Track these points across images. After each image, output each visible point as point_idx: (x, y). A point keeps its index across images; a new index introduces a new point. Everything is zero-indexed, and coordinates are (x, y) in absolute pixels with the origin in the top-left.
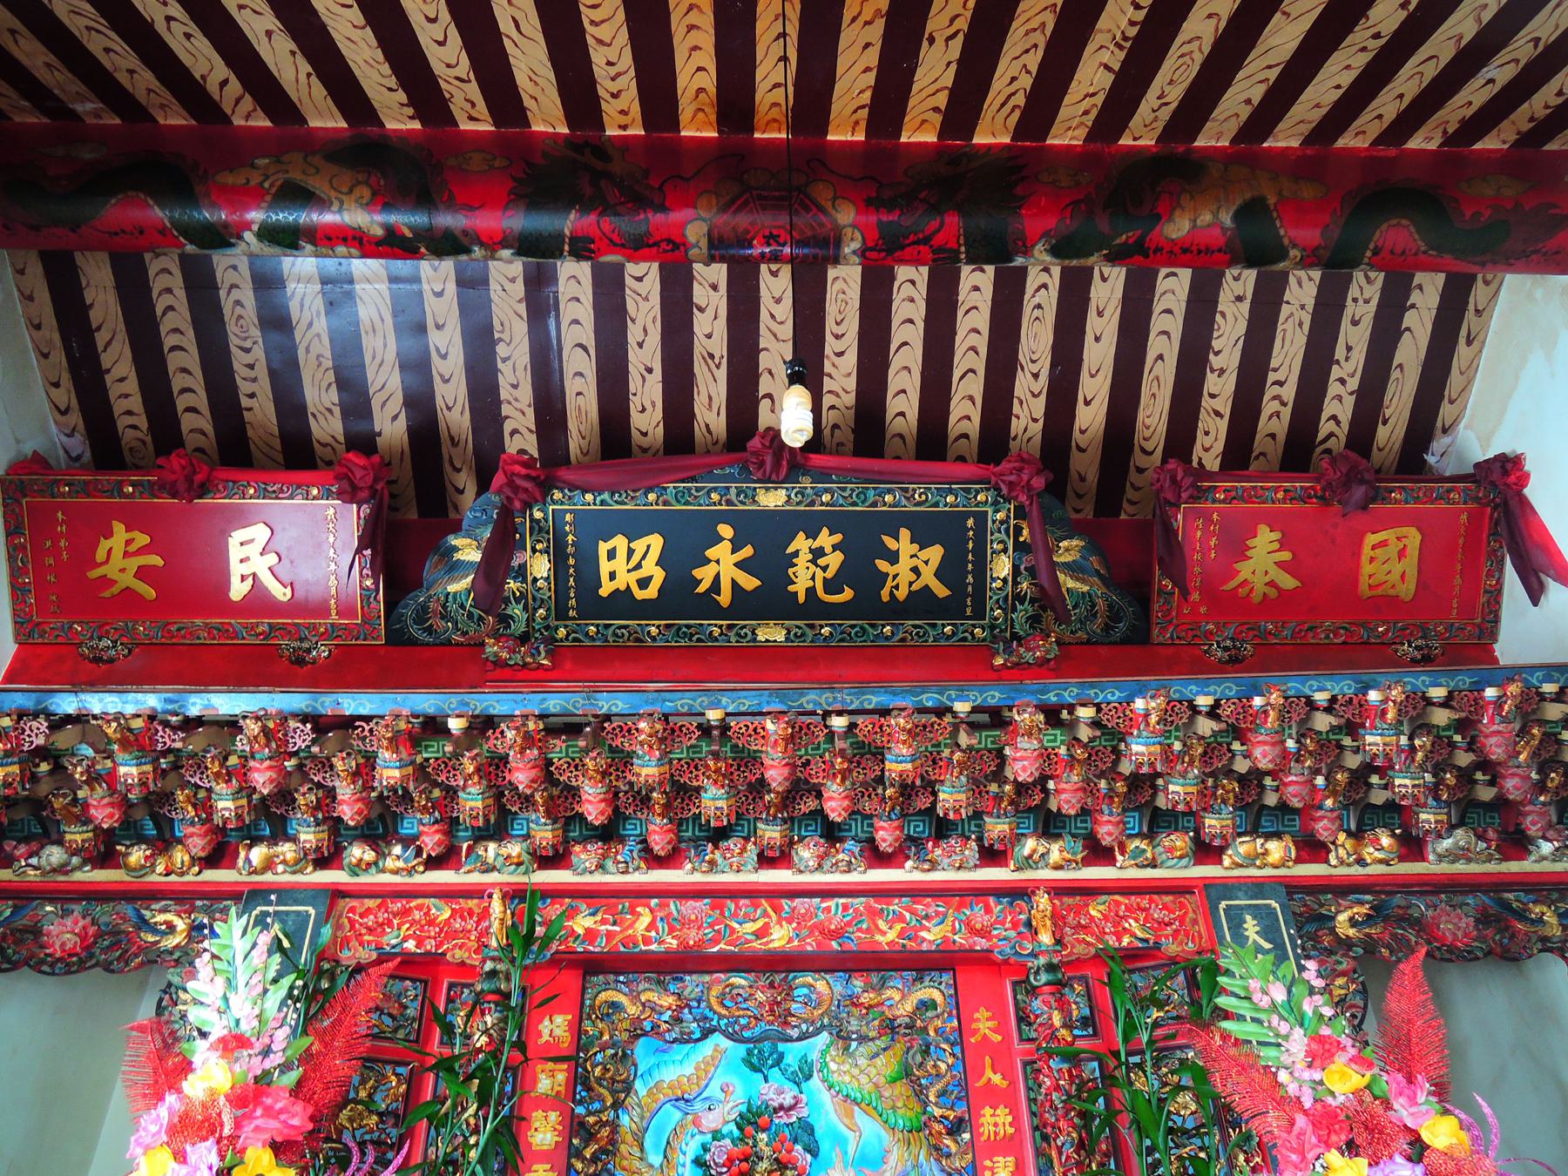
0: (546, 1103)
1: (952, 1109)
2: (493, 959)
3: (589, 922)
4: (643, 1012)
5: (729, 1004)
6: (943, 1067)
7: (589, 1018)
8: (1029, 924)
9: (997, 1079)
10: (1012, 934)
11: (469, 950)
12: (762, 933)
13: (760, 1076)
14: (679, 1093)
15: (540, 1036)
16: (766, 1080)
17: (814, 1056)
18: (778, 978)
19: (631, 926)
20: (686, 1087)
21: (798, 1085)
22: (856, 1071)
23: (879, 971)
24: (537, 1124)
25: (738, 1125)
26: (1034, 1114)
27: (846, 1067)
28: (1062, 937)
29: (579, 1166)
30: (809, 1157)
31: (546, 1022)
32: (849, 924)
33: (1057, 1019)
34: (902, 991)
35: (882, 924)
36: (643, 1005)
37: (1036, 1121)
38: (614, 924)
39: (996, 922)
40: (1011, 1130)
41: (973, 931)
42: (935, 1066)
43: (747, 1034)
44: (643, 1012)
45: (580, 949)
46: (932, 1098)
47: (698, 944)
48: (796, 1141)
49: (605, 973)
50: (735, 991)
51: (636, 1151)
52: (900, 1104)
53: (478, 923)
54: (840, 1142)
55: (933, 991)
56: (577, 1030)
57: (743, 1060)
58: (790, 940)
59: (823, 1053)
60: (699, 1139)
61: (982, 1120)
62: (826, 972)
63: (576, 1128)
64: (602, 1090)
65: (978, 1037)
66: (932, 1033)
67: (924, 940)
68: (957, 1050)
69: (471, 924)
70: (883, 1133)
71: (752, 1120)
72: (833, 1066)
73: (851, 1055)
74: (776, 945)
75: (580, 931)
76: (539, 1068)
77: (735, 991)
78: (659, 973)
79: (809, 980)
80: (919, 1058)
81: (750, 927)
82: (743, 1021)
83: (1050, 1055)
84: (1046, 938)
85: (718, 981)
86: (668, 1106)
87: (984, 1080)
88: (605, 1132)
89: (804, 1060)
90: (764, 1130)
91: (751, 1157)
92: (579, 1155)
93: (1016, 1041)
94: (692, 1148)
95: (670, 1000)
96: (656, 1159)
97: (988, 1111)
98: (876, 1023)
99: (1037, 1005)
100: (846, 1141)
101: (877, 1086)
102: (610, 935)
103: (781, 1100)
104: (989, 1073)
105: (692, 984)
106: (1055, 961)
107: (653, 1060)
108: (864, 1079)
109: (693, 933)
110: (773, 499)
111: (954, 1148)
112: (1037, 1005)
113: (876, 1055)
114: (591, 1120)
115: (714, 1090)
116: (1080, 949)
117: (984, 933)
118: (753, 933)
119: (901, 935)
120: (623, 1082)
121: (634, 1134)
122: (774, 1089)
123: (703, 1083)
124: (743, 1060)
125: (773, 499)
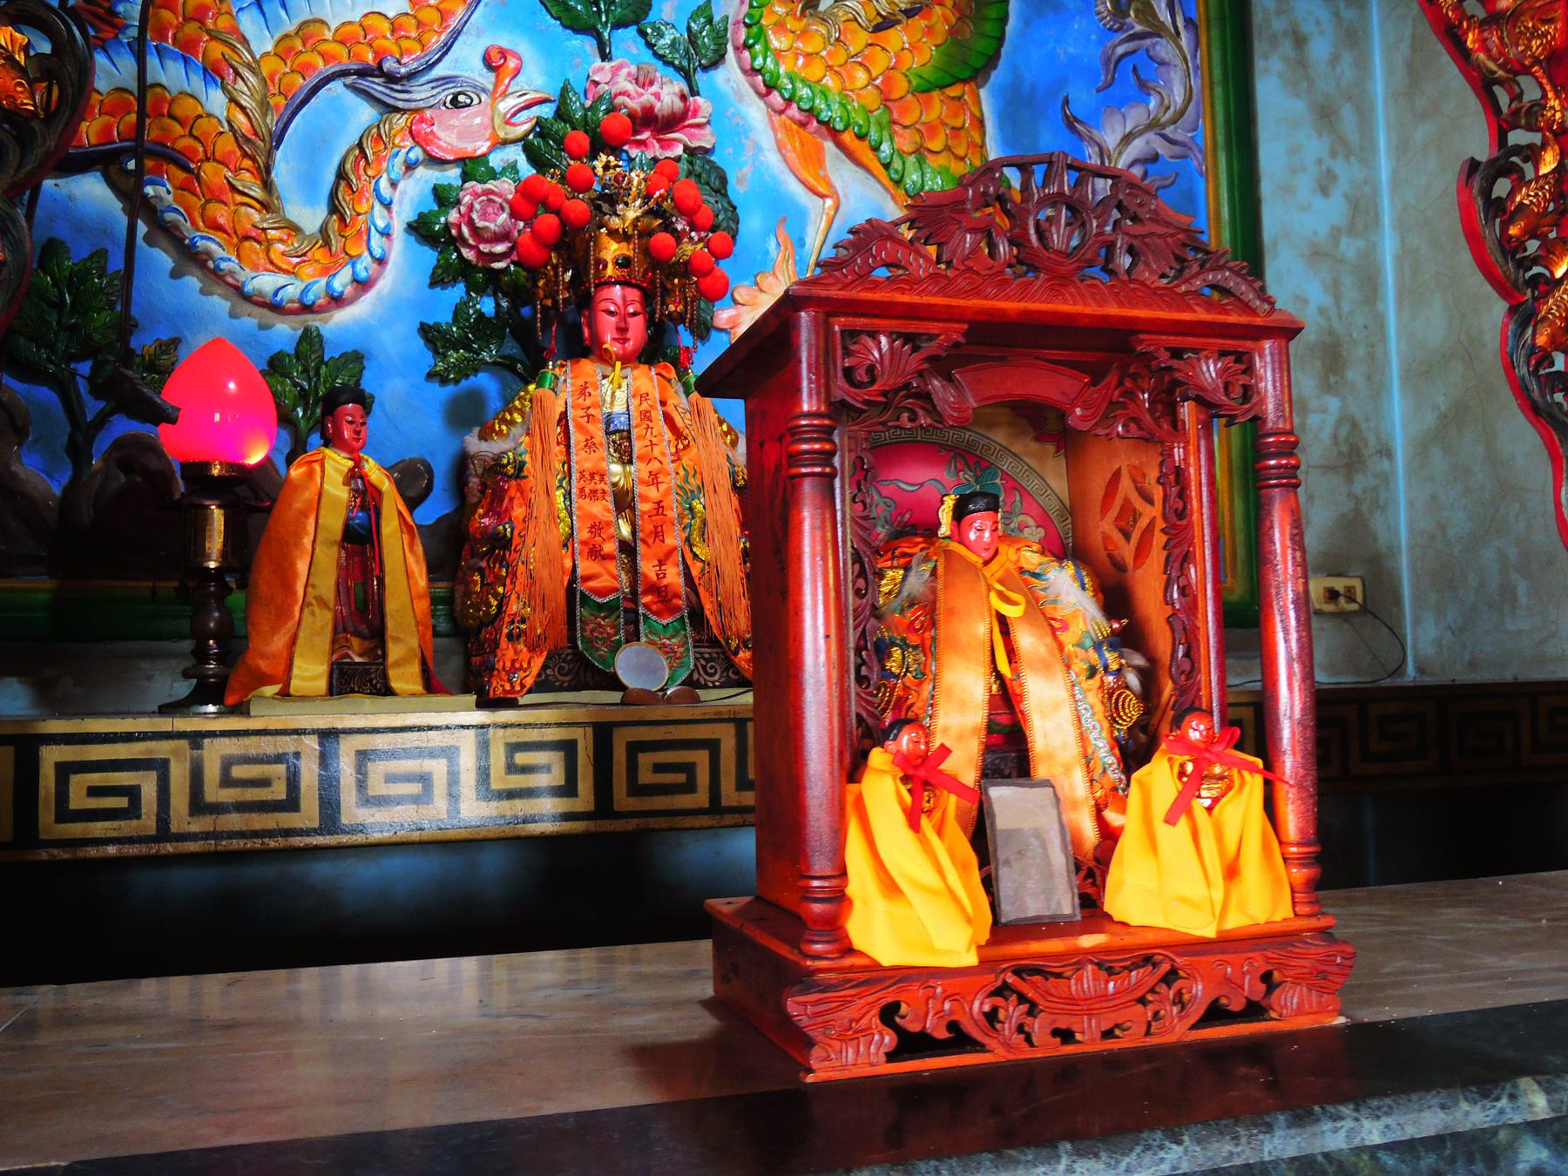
13: (587, 44)
20: (388, 44)
25: (529, 150)
51: (248, 182)
60: (428, 176)
71: (573, 136)
86: (337, 86)
94: (411, 194)
96: (311, 216)
100: (802, 216)
103: (647, 97)
110: (1088, 941)
115: (465, 61)
122: (625, 74)
125: (1088, 941)
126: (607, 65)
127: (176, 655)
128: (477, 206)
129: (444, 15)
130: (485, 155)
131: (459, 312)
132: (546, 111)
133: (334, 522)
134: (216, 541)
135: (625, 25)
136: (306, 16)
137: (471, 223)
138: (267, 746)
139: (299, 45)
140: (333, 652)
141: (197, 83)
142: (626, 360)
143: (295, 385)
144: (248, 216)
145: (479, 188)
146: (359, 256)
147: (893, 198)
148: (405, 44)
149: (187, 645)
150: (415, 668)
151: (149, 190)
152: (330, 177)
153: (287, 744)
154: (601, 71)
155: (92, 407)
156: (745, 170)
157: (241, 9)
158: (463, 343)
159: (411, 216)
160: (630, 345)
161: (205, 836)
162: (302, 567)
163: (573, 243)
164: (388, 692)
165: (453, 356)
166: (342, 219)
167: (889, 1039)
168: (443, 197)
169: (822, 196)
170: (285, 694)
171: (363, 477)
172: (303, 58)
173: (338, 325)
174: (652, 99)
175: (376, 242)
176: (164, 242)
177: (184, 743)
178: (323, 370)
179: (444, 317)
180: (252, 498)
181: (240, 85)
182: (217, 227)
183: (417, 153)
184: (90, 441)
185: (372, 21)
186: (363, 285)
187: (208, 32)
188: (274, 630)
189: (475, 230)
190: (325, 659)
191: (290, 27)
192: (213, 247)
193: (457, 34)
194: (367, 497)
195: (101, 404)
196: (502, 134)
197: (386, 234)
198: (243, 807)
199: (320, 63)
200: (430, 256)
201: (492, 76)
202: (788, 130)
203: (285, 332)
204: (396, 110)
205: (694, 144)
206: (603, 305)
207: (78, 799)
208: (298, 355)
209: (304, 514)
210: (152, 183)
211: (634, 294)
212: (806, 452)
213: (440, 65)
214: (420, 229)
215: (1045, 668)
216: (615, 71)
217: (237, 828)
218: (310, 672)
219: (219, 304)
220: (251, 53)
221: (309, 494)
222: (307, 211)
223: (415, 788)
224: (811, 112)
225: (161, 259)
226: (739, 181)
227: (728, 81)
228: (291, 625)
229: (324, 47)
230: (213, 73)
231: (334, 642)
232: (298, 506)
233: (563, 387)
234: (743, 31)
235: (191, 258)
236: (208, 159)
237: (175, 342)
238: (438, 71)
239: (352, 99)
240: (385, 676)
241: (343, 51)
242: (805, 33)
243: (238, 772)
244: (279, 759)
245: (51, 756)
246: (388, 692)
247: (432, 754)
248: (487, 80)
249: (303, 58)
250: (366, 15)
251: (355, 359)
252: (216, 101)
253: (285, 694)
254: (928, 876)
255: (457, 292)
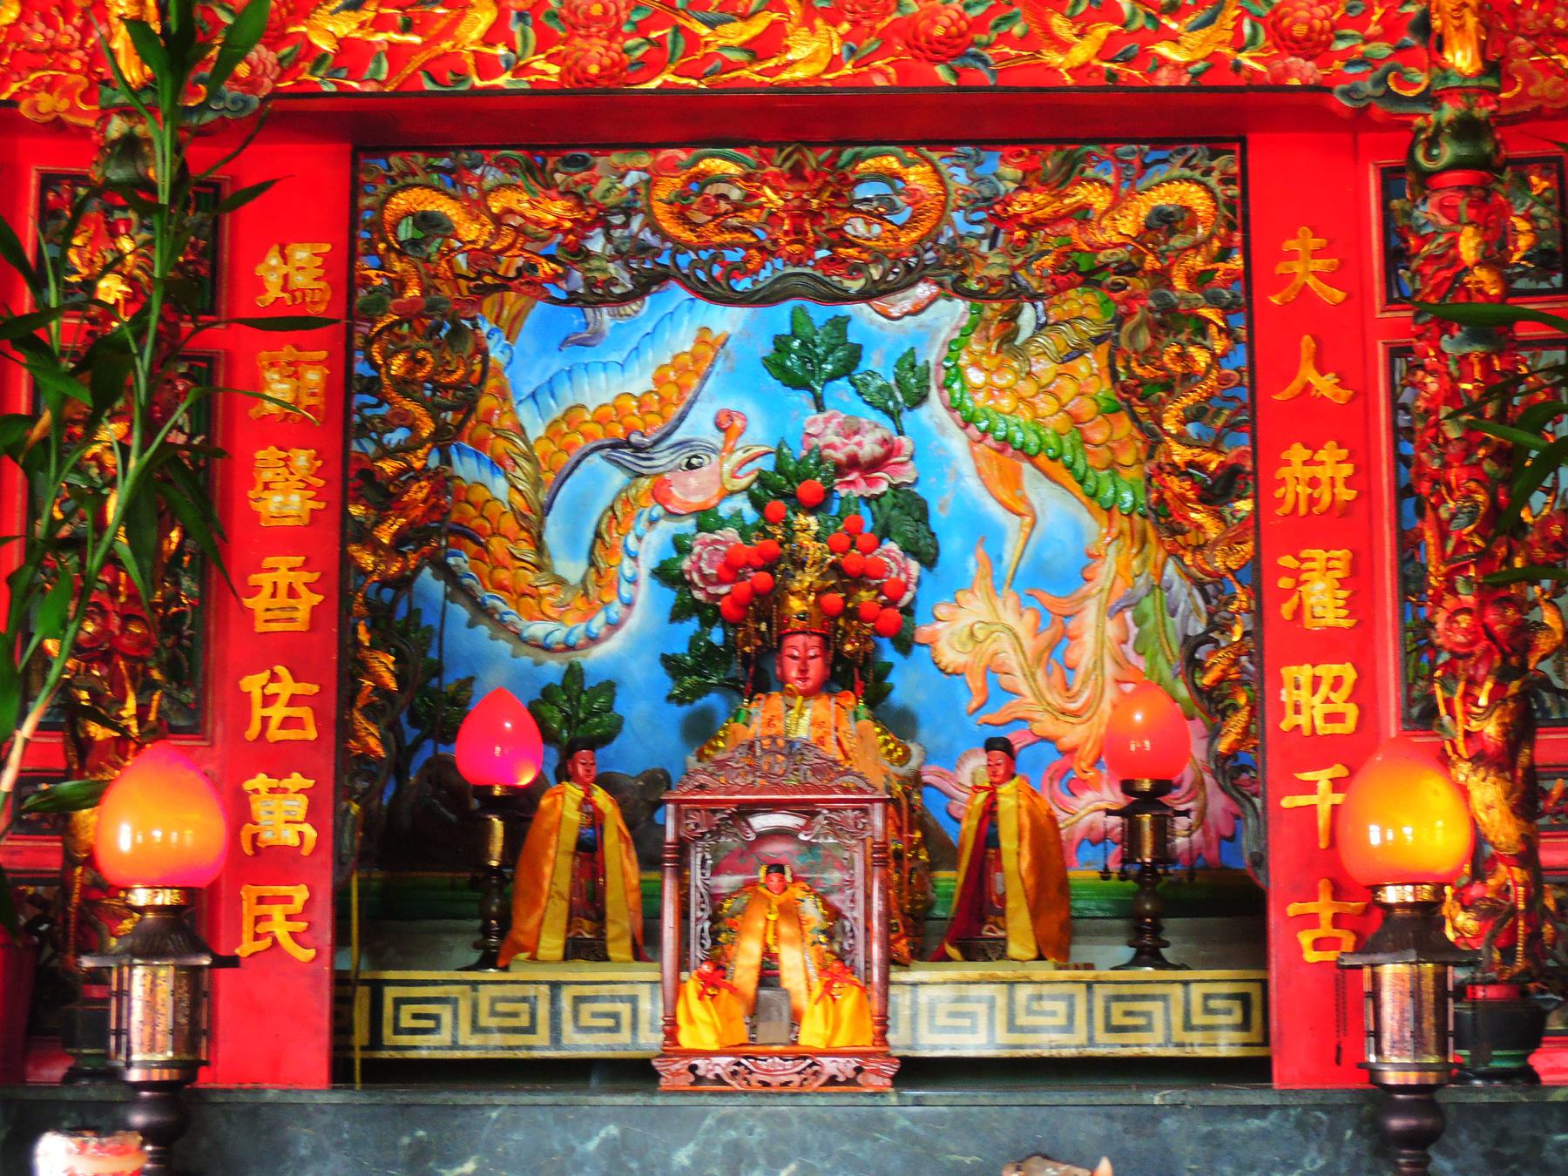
0: (286, 431)
1: (1215, 448)
2: (125, 111)
3: (346, 26)
4: (495, 235)
5: (701, 218)
6: (1201, 358)
7: (372, 250)
8: (1423, 26)
9: (1325, 385)
10: (1382, 49)
11: (68, 92)
12: (766, 46)
13: (802, 398)
14: (620, 432)
15: (263, 291)
16: (820, 406)
17: (931, 355)
18: (812, 159)
19: (447, 33)
21: (893, 415)
22: (1028, 388)
23: (1059, 142)
24: (267, 475)
25: (757, 503)
26: (1406, 460)
27: (1006, 379)
28: (1505, 59)
29: (367, 560)
30: (914, 567)
31: (273, 260)
32: (979, 24)
33: (1469, 246)
34: (1114, 189)
35: (1060, 25)
36: (498, 220)
37: (1406, 475)
38: (408, 28)
39: (1345, 21)
40: (1347, 495)
41: (1284, 41)
42: (1182, 356)
43: (744, 284)
44: (495, 235)
45: (329, 88)
46: (1170, 426)
47: (612, 71)
48: (885, 533)
49: (405, 148)
50: (712, 190)
51: (526, 551)
52: (1127, 458)
53: (85, 30)
54: (984, 536)
55: (1181, 189)
56: (343, 273)
57: (767, 363)
58: (835, 63)
59: (953, 347)
60: (668, 528)
61: (1284, 472)
62: (933, 144)
63: (351, 482)
64: (410, 406)
65: (1290, 293)
66: (1180, 284)
67: (1164, 61)
68: (1239, 323)
69: (67, 33)
70: (1086, 519)
71: (786, 487)
72: (976, 377)
73: (1020, 353)
74: (800, 73)
75: (325, 45)
76: (264, 356)
77: (712, 190)
78: (531, 149)
79: (892, 163)
80: (1144, 338)
81: (738, 33)
82: (734, 256)
83: (1444, 325)
84: (1462, 58)
85: (672, 167)
86: (595, 458)
87: (1295, 386)
88: (419, 492)
89: (908, 363)
90: (811, 510)
91: (780, 561)
92: (364, 536)
93: (1378, 302)
94: (650, 544)
95: (556, 210)
96: (571, 568)
97: (1297, 453)
98: (1048, 260)
99: (1426, 212)
100: (999, 533)
101: (1076, 420)
102: (396, 54)
103: (851, 448)
104: (1308, 374)
105: (620, 174)
106: (1482, 113)
107: (557, 363)
108: (1046, 406)
109: (597, 47)
111: (1212, 530)
112: (1426, 212)
113: (1078, 352)
114: (389, 466)
115: (700, 425)
116: (1544, 87)
117: (1314, 47)
118: (745, 47)
119: (1104, 52)
120: (455, 386)
121: (519, 515)
122: (840, 423)
123: (675, 412)
124: (767, 363)
126: (821, 416)
127: (464, 932)
128: (705, 556)
129: (682, 388)
130: (715, 507)
131: (693, 643)
132: (767, 464)
133: (569, 838)
134: (497, 846)
135: (838, 378)
136: (571, 403)
137: (700, 570)
138: (517, 991)
139: (564, 428)
140: (568, 931)
141: (485, 474)
142: (807, 694)
143: (562, 711)
144: (525, 577)
145: (709, 537)
146: (610, 603)
147: (1089, 511)
148: (649, 418)
149: (478, 923)
150: (627, 943)
151: (451, 561)
152: (589, 535)
153: (530, 991)
154: (812, 420)
155: (411, 734)
156: (947, 496)
157: (520, 402)
158: (695, 670)
159: (654, 564)
160: (810, 684)
161: (480, 1048)
162: (547, 870)
163: (768, 603)
164: (606, 959)
165: (688, 681)
166: (598, 572)
167: (692, 1078)
168: (680, 545)
169: (1020, 515)
170: (533, 958)
171: (592, 803)
172: (569, 438)
173: (595, 659)
174: (855, 448)
175: (626, 590)
176: (462, 598)
177: (467, 987)
178: (584, 698)
179: (680, 648)
180: (521, 808)
181: (519, 473)
182: (501, 587)
183: (658, 511)
184: (408, 761)
185: (624, 401)
186: (613, 626)
187: (494, 430)
188: (529, 915)
189: (703, 577)
190: (562, 934)
191: (557, 413)
192: (499, 603)
193: (691, 404)
194: (595, 819)
195: (417, 732)
196: (729, 487)
197: (633, 581)
198: (503, 1030)
199: (580, 439)
200: (670, 596)
201: (722, 436)
202: (989, 458)
203: (554, 667)
204: (641, 475)
205: (897, 480)
206: (789, 651)
207: (406, 1021)
208: (564, 687)
209: (549, 833)
210: (454, 555)
211: (815, 640)
212: (88, 1055)
213: (680, 430)
214: (665, 574)
215: (791, 941)
216: (827, 421)
217: (499, 1044)
218: (552, 944)
219: (504, 646)
220: (526, 442)
221: (553, 818)
222: (572, 565)
223: (610, 1022)
224: (1006, 441)
225: (461, 612)
226: (942, 507)
227: (931, 416)
228: (540, 912)
229: (585, 427)
230: (497, 464)
231: (569, 923)
232: (546, 826)
233: (760, 718)
234: (943, 372)
235: (482, 611)
236: (494, 534)
237: (471, 680)
238: (678, 436)
239: (606, 465)
240: (604, 948)
241: (598, 429)
242: (999, 368)
243: (500, 1007)
244: (524, 999)
245: (390, 993)
246: (606, 959)
247: (621, 999)
248: (717, 439)
249: (569, 438)
250: (618, 397)
251: (609, 688)
252: (500, 487)
253: (533, 958)
254: (708, 1019)
255: (692, 625)
